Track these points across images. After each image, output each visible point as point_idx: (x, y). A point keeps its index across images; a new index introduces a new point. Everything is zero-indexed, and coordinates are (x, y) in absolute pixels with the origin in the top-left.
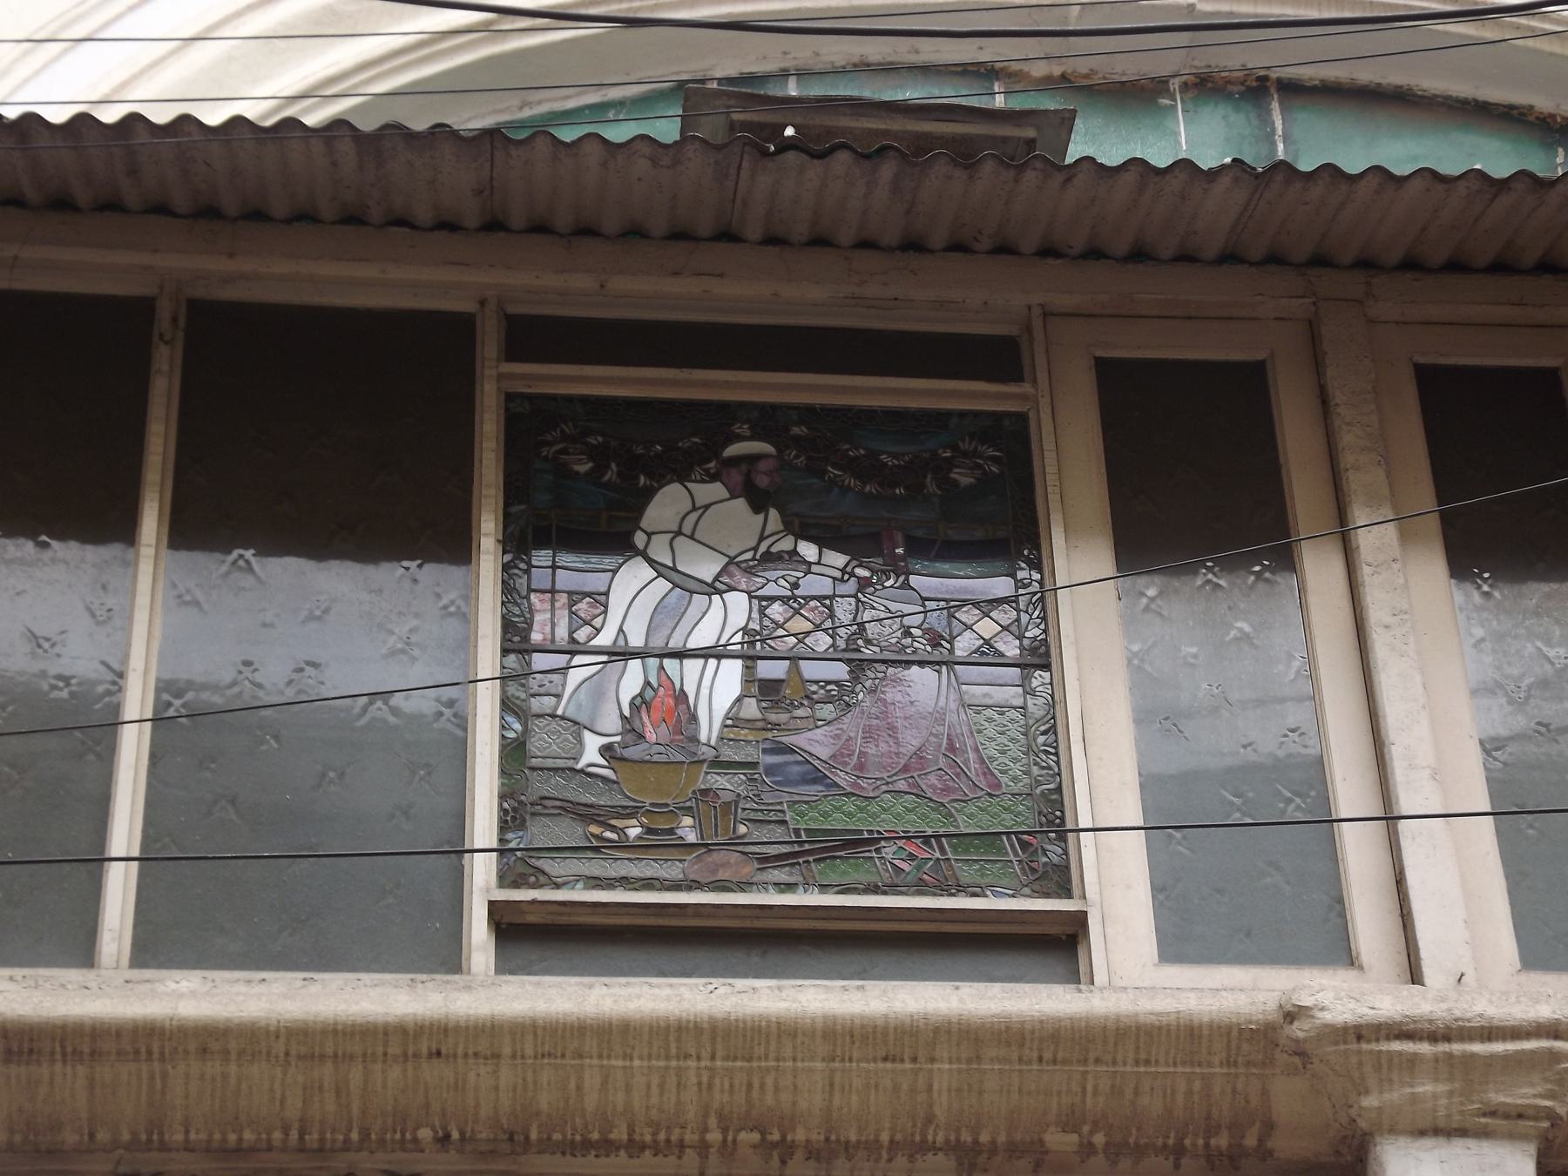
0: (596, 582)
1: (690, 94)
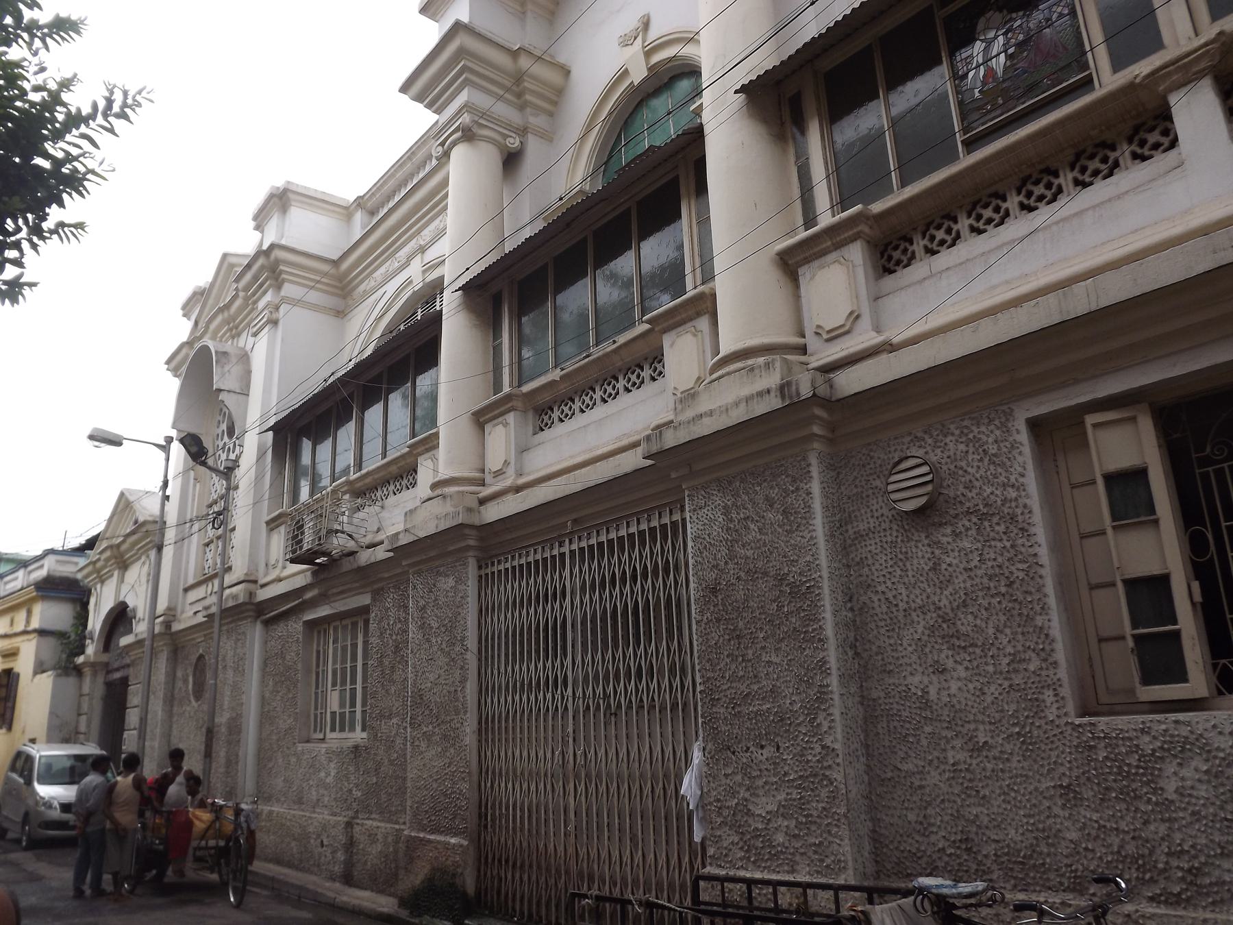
0: (969, 52)
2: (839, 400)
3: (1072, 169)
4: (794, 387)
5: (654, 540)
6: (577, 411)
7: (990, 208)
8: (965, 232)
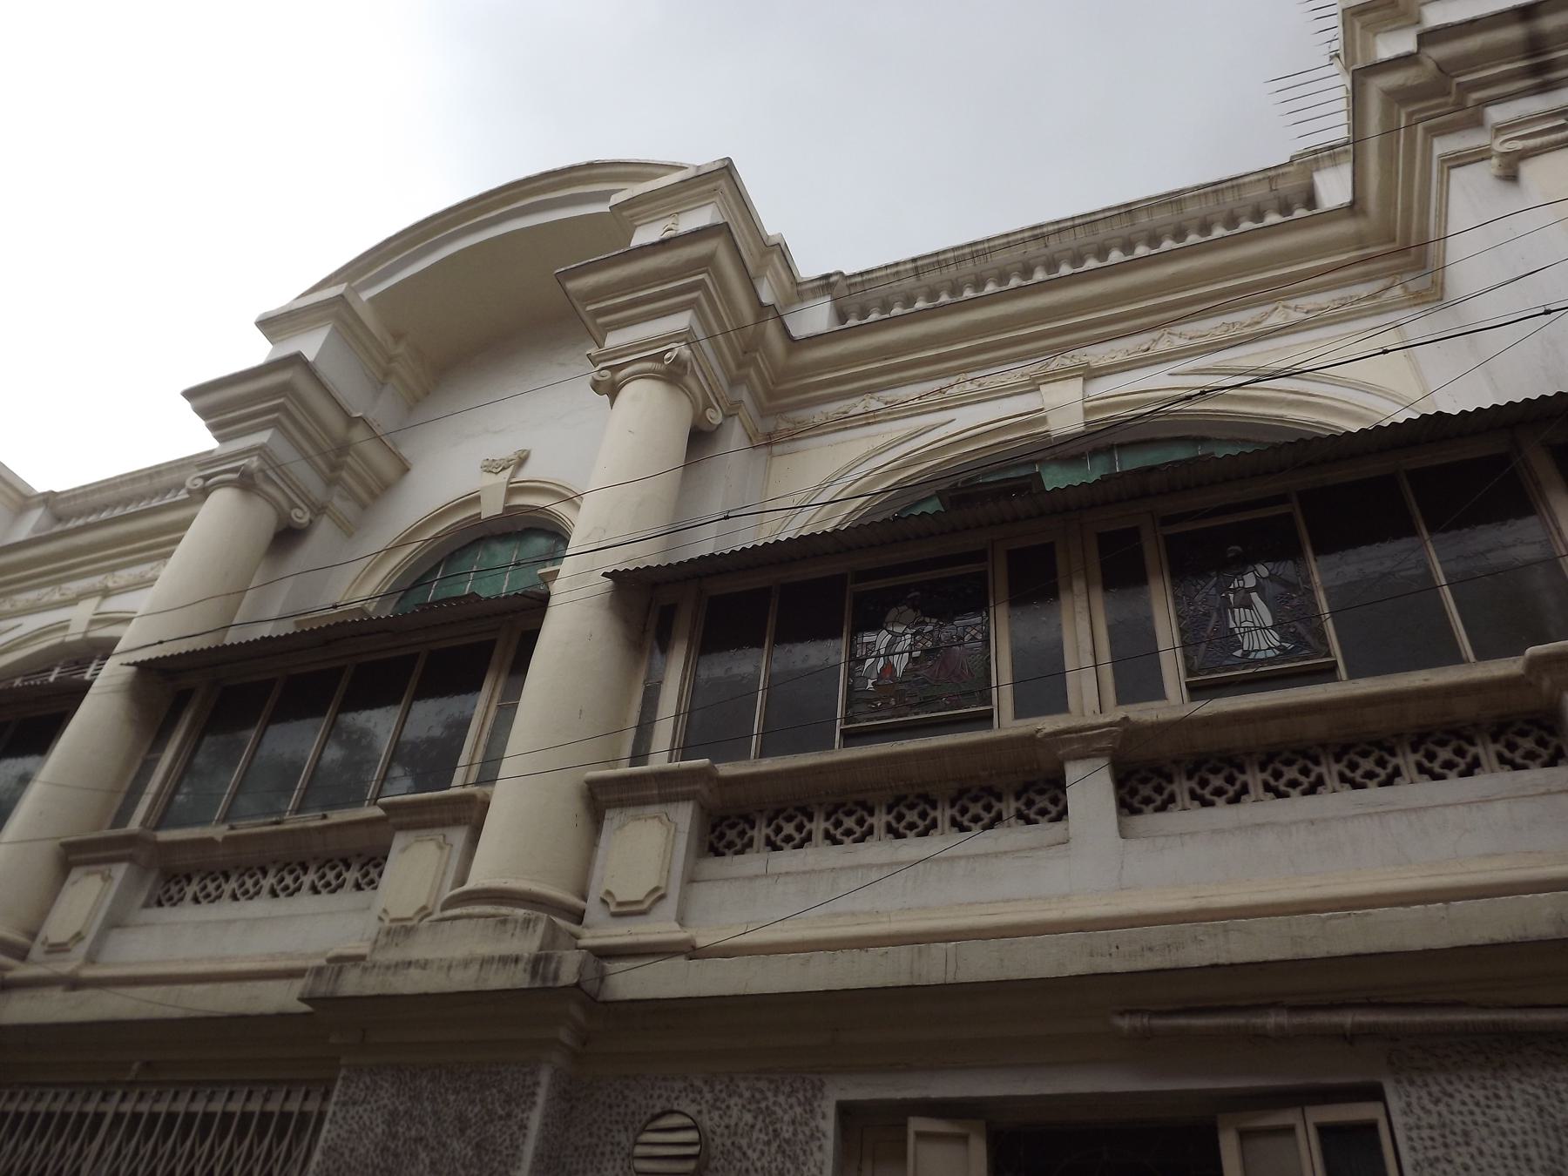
1: (939, 494)
2: (605, 1003)
3: (952, 806)
4: (553, 965)
5: (280, 1134)
6: (306, 887)
7: (854, 818)
8: (818, 836)
